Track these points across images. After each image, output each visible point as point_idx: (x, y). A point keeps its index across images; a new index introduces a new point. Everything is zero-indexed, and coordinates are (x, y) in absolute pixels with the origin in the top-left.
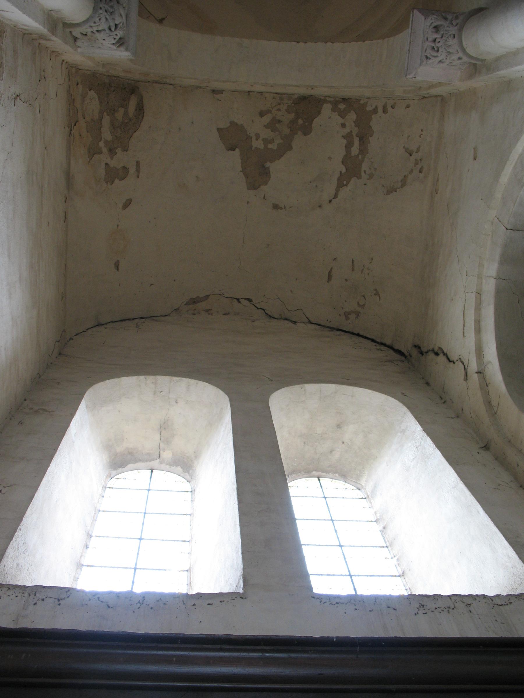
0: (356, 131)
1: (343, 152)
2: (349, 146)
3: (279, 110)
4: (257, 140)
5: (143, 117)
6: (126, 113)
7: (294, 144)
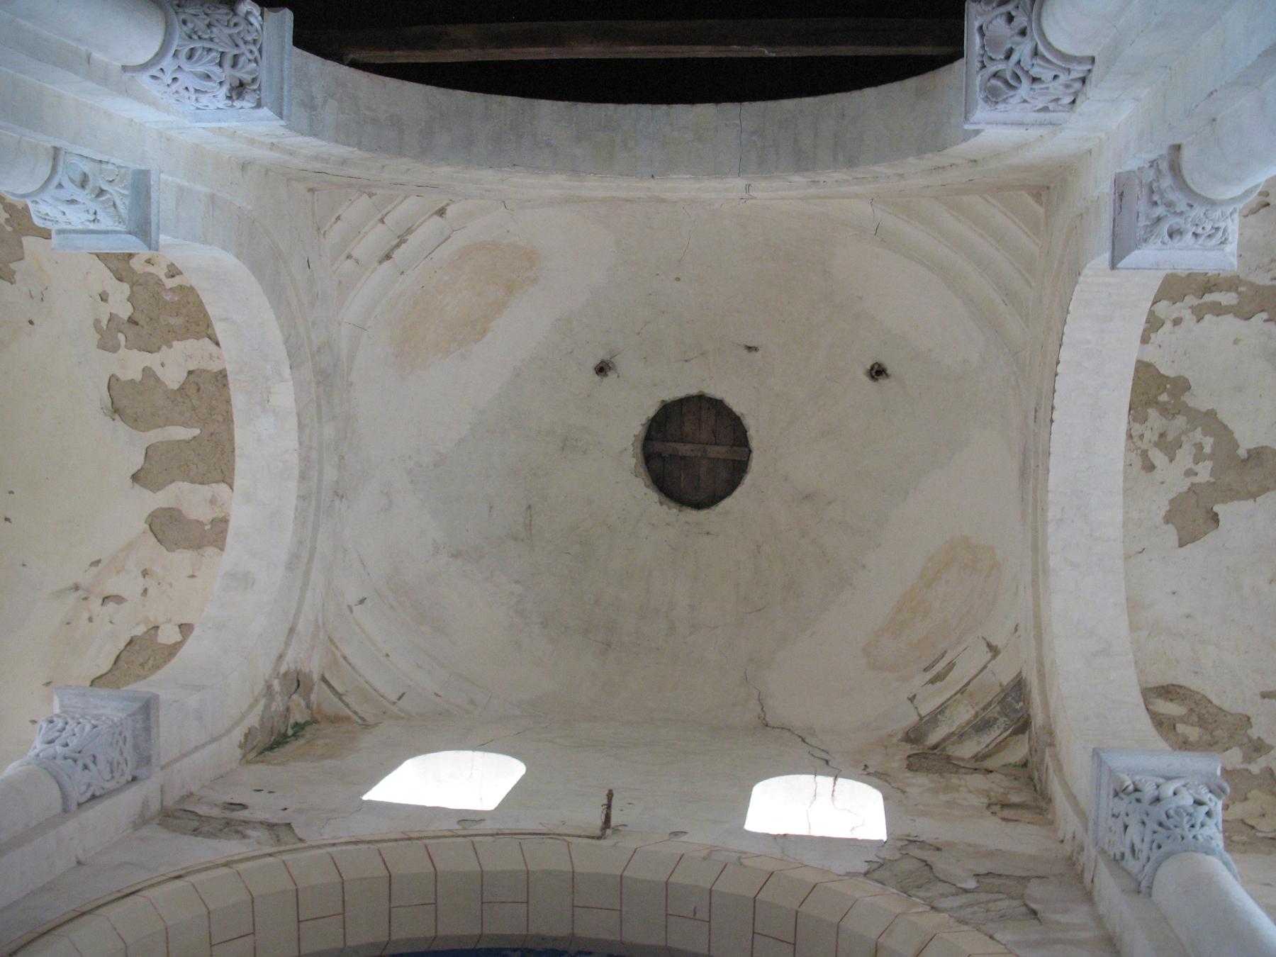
0: (1191, 300)
1: (1230, 318)
2: (1218, 310)
3: (1141, 437)
4: (1196, 474)
5: (1181, 687)
6: (1182, 720)
7: (1204, 407)
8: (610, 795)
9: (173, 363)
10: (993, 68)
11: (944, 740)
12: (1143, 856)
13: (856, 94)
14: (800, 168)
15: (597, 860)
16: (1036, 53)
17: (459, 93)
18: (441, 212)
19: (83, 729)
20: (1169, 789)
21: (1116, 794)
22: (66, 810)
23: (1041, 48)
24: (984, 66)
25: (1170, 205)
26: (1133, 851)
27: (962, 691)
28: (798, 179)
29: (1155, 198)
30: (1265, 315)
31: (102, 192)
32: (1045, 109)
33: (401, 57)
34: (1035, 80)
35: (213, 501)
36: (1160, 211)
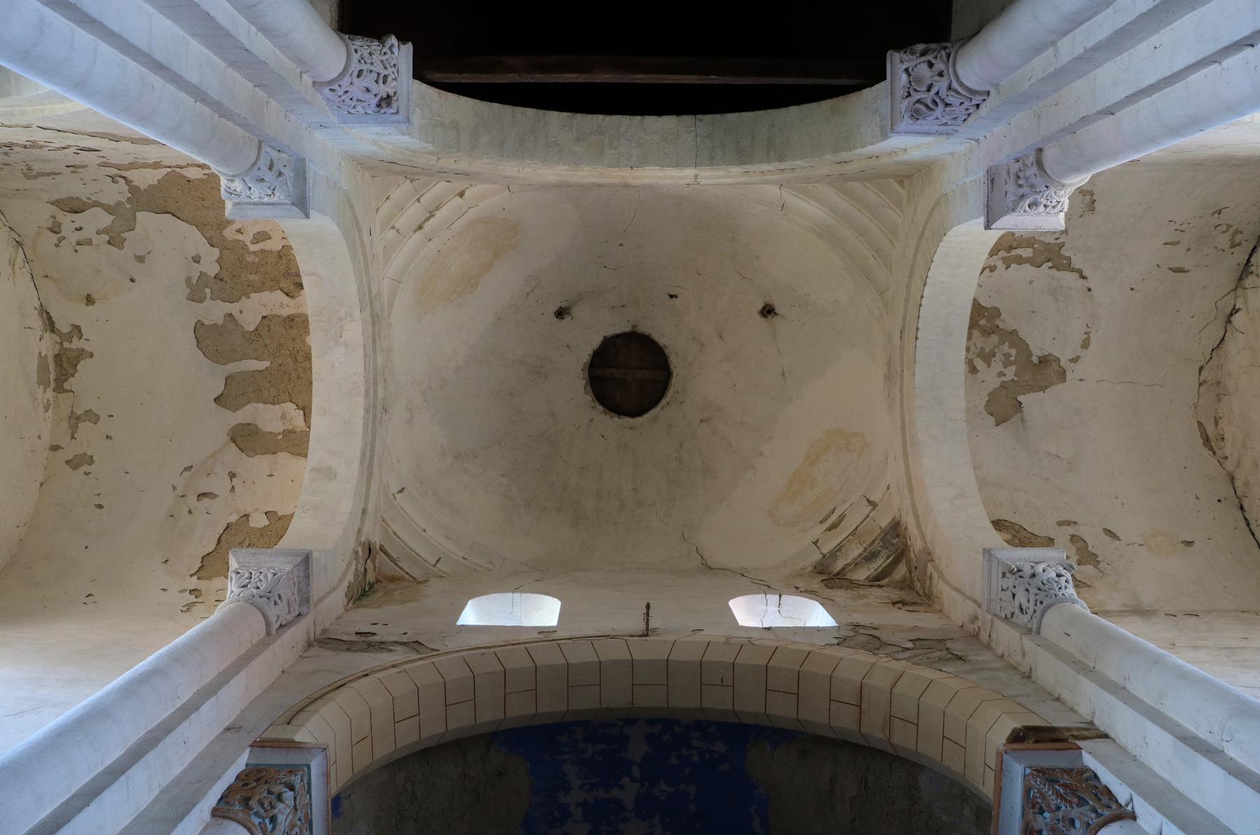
1: (1027, 266)
2: (1020, 260)
8: (648, 606)
9: (254, 309)
10: (916, 96)
11: (843, 569)
12: (1031, 611)
13: (783, 111)
14: (741, 162)
15: (643, 651)
16: (950, 88)
17: (495, 105)
18: (461, 195)
19: (266, 576)
20: (1040, 568)
21: (1004, 575)
22: (268, 634)
23: (955, 85)
24: (909, 95)
25: (1032, 186)
26: (1021, 609)
27: (853, 533)
28: (736, 170)
29: (1020, 182)
30: (1050, 264)
31: (280, 174)
32: (946, 124)
33: (438, 76)
34: (947, 105)
35: (283, 417)
36: (1025, 190)
